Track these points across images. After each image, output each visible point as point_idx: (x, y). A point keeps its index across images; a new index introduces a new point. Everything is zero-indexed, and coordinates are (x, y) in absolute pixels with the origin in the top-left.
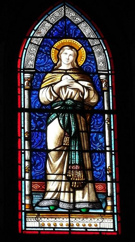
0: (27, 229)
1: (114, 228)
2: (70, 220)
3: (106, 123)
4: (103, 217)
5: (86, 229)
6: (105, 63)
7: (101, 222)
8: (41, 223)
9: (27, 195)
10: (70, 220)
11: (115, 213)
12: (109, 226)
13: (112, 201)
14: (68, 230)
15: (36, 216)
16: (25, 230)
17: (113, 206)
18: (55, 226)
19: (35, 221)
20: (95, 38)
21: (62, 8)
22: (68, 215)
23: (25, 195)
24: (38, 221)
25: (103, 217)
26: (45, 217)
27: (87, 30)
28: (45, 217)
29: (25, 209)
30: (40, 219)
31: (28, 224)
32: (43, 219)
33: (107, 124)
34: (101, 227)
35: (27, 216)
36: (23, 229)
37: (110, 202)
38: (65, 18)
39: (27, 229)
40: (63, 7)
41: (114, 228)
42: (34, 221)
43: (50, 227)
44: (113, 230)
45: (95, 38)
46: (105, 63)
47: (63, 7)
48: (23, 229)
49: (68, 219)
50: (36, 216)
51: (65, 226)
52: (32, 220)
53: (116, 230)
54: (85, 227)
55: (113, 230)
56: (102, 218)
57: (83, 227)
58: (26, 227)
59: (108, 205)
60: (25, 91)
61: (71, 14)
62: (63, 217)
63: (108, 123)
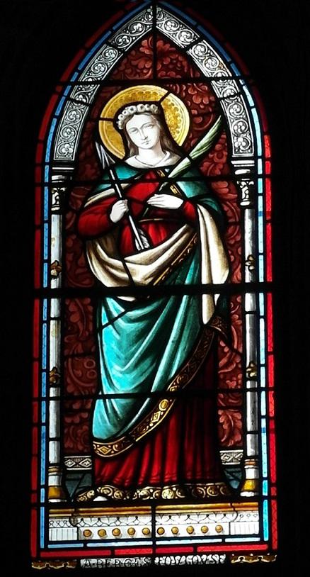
0: (50, 546)
1: (261, 534)
2: (154, 522)
3: (247, 267)
4: (236, 509)
5: (224, 537)
6: (243, 105)
7: (232, 520)
8: (82, 529)
9: (53, 465)
10: (154, 522)
11: (273, 496)
12: (247, 528)
13: (258, 466)
14: (151, 543)
15: (70, 515)
16: (46, 549)
17: (259, 481)
18: (173, 533)
19: (69, 524)
20: (229, 78)
21: (149, 10)
22: (150, 507)
23: (48, 464)
24: (75, 526)
25: (236, 509)
26: (108, 513)
27: (210, 63)
28: (108, 513)
29: (47, 498)
30: (79, 520)
31: (55, 535)
32: (87, 520)
33: (249, 270)
34: (232, 533)
35: (50, 516)
36: (42, 546)
37: (254, 470)
38: (155, 34)
39: (50, 546)
40: (151, 7)
41: (261, 534)
42: (66, 526)
43: (192, 535)
44: (257, 539)
45: (229, 78)
46: (243, 105)
47: (151, 7)
48: (42, 546)
49: (149, 519)
50: (70, 515)
51: (139, 535)
52: (62, 524)
53: (266, 539)
54: (221, 534)
55: (257, 539)
56: (234, 511)
57: (217, 534)
58: (47, 542)
59: (247, 478)
60: (53, 216)
61: (168, 26)
62: (189, 511)
63: (251, 268)
